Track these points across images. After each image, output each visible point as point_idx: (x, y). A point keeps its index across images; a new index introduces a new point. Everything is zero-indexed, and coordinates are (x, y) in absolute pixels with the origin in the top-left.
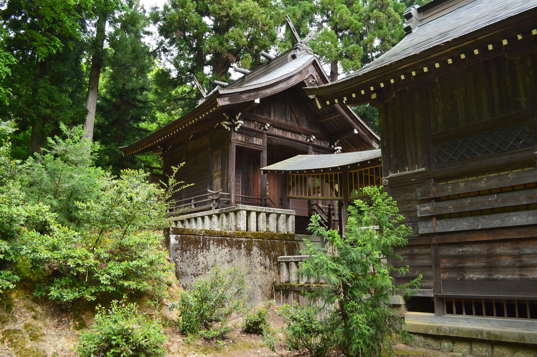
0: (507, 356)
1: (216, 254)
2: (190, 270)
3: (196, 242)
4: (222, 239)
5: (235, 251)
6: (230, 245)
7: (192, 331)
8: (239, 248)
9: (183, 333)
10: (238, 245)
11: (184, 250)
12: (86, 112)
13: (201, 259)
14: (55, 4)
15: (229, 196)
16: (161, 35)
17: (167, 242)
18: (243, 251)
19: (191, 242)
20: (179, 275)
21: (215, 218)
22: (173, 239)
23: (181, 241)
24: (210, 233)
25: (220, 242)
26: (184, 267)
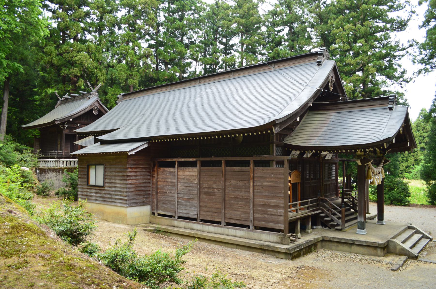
0: (117, 2)
1: (52, 175)
2: (43, 179)
3: (45, 172)
4: (53, 170)
5: (58, 174)
6: (56, 172)
7: (40, 194)
8: (59, 172)
9: (38, 194)
10: (59, 172)
11: (41, 174)
12: (4, 101)
13: (46, 176)
14: (407, 84)
15: (62, 152)
16: (406, 184)
17: (36, 171)
18: (61, 173)
19: (43, 171)
20: (39, 181)
21: (54, 162)
22: (38, 171)
23: (40, 171)
24: (49, 169)
25: (53, 171)
26: (41, 179)
